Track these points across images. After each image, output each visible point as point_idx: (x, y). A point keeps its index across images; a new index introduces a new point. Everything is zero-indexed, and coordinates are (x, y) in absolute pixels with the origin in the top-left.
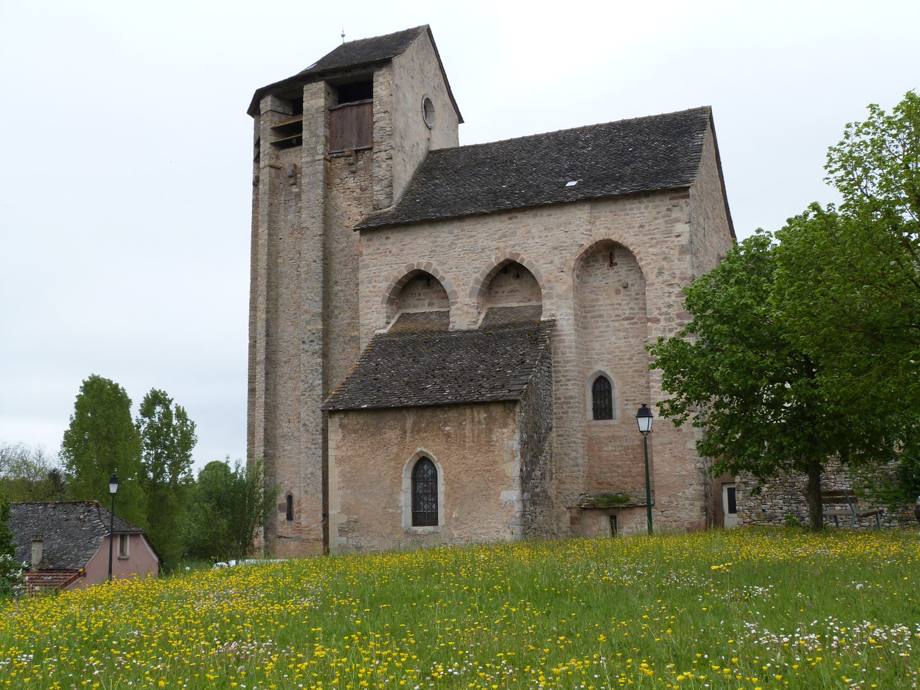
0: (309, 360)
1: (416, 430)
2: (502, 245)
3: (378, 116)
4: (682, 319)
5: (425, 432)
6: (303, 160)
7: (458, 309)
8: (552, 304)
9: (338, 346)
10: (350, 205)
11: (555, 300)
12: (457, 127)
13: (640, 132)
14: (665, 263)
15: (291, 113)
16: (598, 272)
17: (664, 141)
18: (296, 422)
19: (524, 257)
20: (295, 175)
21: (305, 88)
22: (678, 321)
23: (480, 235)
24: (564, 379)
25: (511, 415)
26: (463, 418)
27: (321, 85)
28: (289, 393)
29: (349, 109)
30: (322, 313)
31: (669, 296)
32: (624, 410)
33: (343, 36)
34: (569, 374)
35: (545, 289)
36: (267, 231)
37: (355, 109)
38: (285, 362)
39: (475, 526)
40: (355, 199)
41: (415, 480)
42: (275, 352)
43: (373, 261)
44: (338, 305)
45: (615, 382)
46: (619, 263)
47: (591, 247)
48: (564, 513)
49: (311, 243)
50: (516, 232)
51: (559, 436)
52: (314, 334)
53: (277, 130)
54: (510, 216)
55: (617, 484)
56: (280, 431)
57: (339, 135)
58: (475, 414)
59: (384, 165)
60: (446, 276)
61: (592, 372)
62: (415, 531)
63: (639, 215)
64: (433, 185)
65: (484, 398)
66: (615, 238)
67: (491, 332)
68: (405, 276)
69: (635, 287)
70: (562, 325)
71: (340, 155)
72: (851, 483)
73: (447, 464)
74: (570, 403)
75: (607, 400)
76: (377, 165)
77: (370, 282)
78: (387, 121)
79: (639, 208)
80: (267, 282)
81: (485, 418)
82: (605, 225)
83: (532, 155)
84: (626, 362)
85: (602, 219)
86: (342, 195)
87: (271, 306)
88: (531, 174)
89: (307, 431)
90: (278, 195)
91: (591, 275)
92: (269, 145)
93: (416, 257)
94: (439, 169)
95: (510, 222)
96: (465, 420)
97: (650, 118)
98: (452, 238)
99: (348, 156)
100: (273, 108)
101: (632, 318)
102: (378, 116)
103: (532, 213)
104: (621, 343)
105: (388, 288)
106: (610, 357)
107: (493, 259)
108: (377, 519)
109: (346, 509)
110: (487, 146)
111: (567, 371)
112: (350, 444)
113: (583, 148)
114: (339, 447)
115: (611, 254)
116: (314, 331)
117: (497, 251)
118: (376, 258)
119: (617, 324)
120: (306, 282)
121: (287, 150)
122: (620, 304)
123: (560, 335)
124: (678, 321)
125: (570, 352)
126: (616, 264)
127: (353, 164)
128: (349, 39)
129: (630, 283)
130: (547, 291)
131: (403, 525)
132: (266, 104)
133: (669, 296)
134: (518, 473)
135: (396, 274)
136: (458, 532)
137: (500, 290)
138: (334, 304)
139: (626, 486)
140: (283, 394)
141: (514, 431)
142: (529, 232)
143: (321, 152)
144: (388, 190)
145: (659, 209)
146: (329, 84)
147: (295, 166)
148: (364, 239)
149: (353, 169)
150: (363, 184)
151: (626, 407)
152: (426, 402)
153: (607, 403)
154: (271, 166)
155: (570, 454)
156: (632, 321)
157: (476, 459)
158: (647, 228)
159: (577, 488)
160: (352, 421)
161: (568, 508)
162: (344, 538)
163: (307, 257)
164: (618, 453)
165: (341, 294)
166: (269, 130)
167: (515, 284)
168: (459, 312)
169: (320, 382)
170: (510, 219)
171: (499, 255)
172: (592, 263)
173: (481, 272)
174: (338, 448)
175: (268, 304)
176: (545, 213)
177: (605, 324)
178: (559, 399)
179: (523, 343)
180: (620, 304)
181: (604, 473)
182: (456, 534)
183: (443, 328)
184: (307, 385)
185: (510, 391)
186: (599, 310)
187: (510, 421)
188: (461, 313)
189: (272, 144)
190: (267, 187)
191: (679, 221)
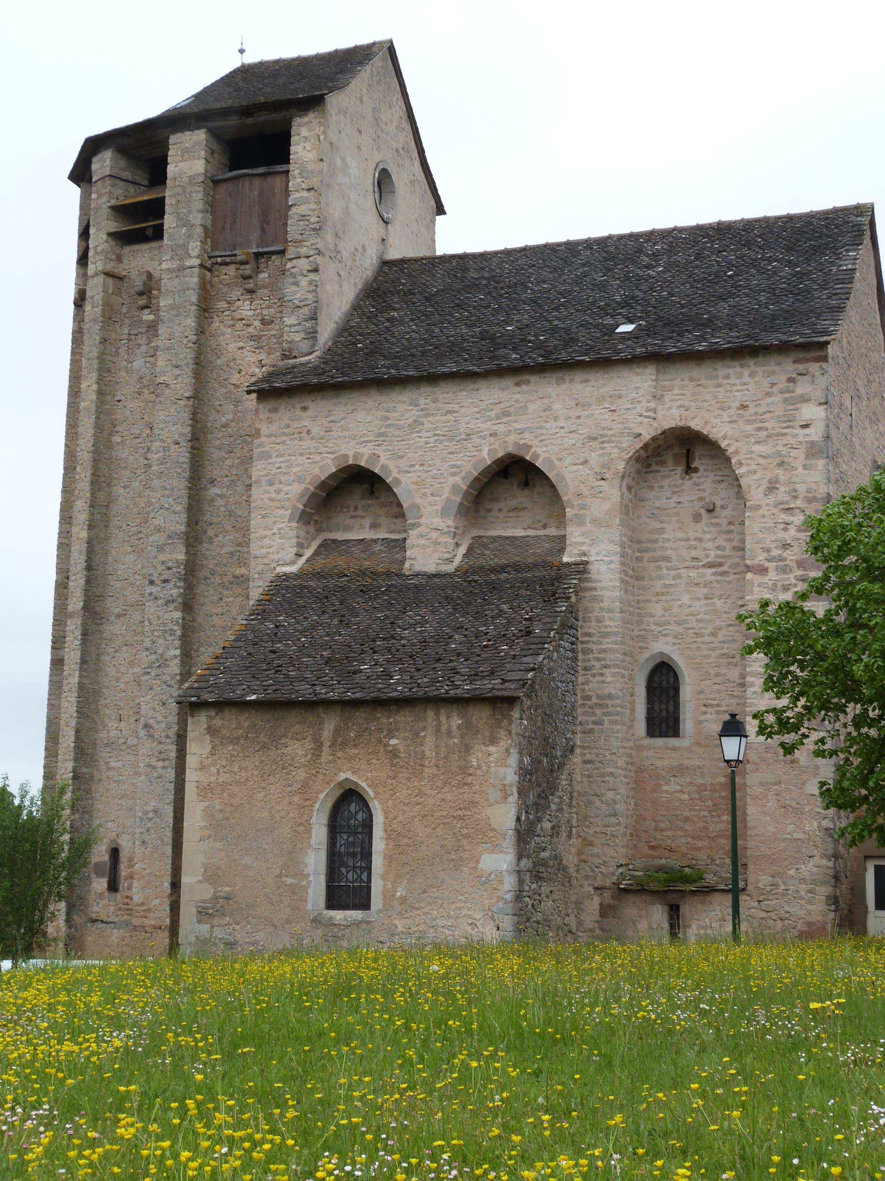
0: (160, 614)
1: (340, 742)
2: (501, 428)
3: (298, 195)
4: (805, 569)
5: (355, 746)
6: (164, 266)
7: (421, 536)
8: (583, 534)
10: (242, 348)
11: (589, 527)
12: (433, 222)
13: (748, 244)
14: (780, 472)
15: (146, 183)
16: (665, 483)
19: (539, 451)
21: (173, 139)
22: (799, 573)
23: (463, 410)
24: (597, 665)
25: (505, 723)
26: (421, 725)
27: (200, 136)
28: (123, 669)
29: (247, 180)
30: (186, 534)
31: (785, 529)
32: (700, 722)
33: (242, 51)
34: (608, 656)
35: (572, 507)
36: (95, 387)
37: (257, 181)
38: (118, 616)
39: (435, 912)
40: (252, 338)
42: (101, 597)
43: (277, 447)
44: (214, 520)
45: (686, 674)
46: (701, 468)
47: (654, 439)
48: (589, 897)
49: (172, 410)
50: (525, 408)
51: (585, 762)
52: (169, 568)
56: (103, 734)
57: (228, 226)
58: (443, 719)
59: (304, 282)
60: (402, 477)
61: (647, 655)
62: (331, 918)
64: (388, 320)
65: (459, 691)
66: (696, 425)
67: (476, 578)
71: (228, 259)
73: (390, 803)
74: (607, 706)
76: (291, 280)
78: (313, 206)
79: (740, 376)
80: (93, 474)
82: (679, 403)
83: (560, 276)
84: (707, 639)
85: (676, 391)
86: (229, 330)
87: (98, 517)
88: (556, 309)
89: (151, 736)
90: (117, 326)
91: (651, 488)
92: (105, 237)
93: (353, 443)
94: (398, 292)
95: (517, 389)
96: (424, 729)
97: (766, 219)
98: (414, 414)
99: (243, 263)
101: (721, 565)
102: (298, 195)
103: (555, 376)
104: (699, 606)
105: (302, 495)
106: (679, 629)
107: (485, 453)
109: (212, 876)
111: (604, 651)
112: (224, 763)
113: (649, 267)
115: (688, 451)
116: (170, 564)
117: (492, 440)
118: (283, 443)
120: (160, 478)
121: (136, 247)
122: (700, 540)
123: (595, 589)
124: (799, 573)
125: (611, 619)
126: (696, 470)
127: (250, 277)
128: (252, 58)
129: (719, 504)
131: (309, 907)
133: (785, 529)
134: (513, 825)
135: (317, 471)
136: (404, 921)
137: (495, 506)
138: (207, 517)
139: (698, 854)
140: (111, 671)
142: (548, 408)
143: (195, 253)
145: (774, 379)
146: (214, 133)
149: (251, 286)
150: (265, 312)
151: (702, 718)
153: (671, 709)
154: (107, 274)
155: (603, 795)
156: (720, 570)
157: (440, 796)
158: (752, 410)
160: (228, 721)
161: (597, 889)
163: (165, 434)
164: (686, 797)
165: (220, 502)
166: (105, 211)
167: (521, 498)
168: (422, 541)
169: (178, 652)
170: (517, 384)
171: (496, 446)
172: (655, 467)
173: (463, 474)
174: (202, 768)
176: (579, 376)
177: (672, 573)
178: (588, 698)
179: (531, 600)
180: (700, 540)
182: (400, 925)
183: (394, 568)
185: (504, 681)
186: (663, 548)
187: (502, 733)
188: (427, 543)
189: (110, 234)
190: (98, 310)
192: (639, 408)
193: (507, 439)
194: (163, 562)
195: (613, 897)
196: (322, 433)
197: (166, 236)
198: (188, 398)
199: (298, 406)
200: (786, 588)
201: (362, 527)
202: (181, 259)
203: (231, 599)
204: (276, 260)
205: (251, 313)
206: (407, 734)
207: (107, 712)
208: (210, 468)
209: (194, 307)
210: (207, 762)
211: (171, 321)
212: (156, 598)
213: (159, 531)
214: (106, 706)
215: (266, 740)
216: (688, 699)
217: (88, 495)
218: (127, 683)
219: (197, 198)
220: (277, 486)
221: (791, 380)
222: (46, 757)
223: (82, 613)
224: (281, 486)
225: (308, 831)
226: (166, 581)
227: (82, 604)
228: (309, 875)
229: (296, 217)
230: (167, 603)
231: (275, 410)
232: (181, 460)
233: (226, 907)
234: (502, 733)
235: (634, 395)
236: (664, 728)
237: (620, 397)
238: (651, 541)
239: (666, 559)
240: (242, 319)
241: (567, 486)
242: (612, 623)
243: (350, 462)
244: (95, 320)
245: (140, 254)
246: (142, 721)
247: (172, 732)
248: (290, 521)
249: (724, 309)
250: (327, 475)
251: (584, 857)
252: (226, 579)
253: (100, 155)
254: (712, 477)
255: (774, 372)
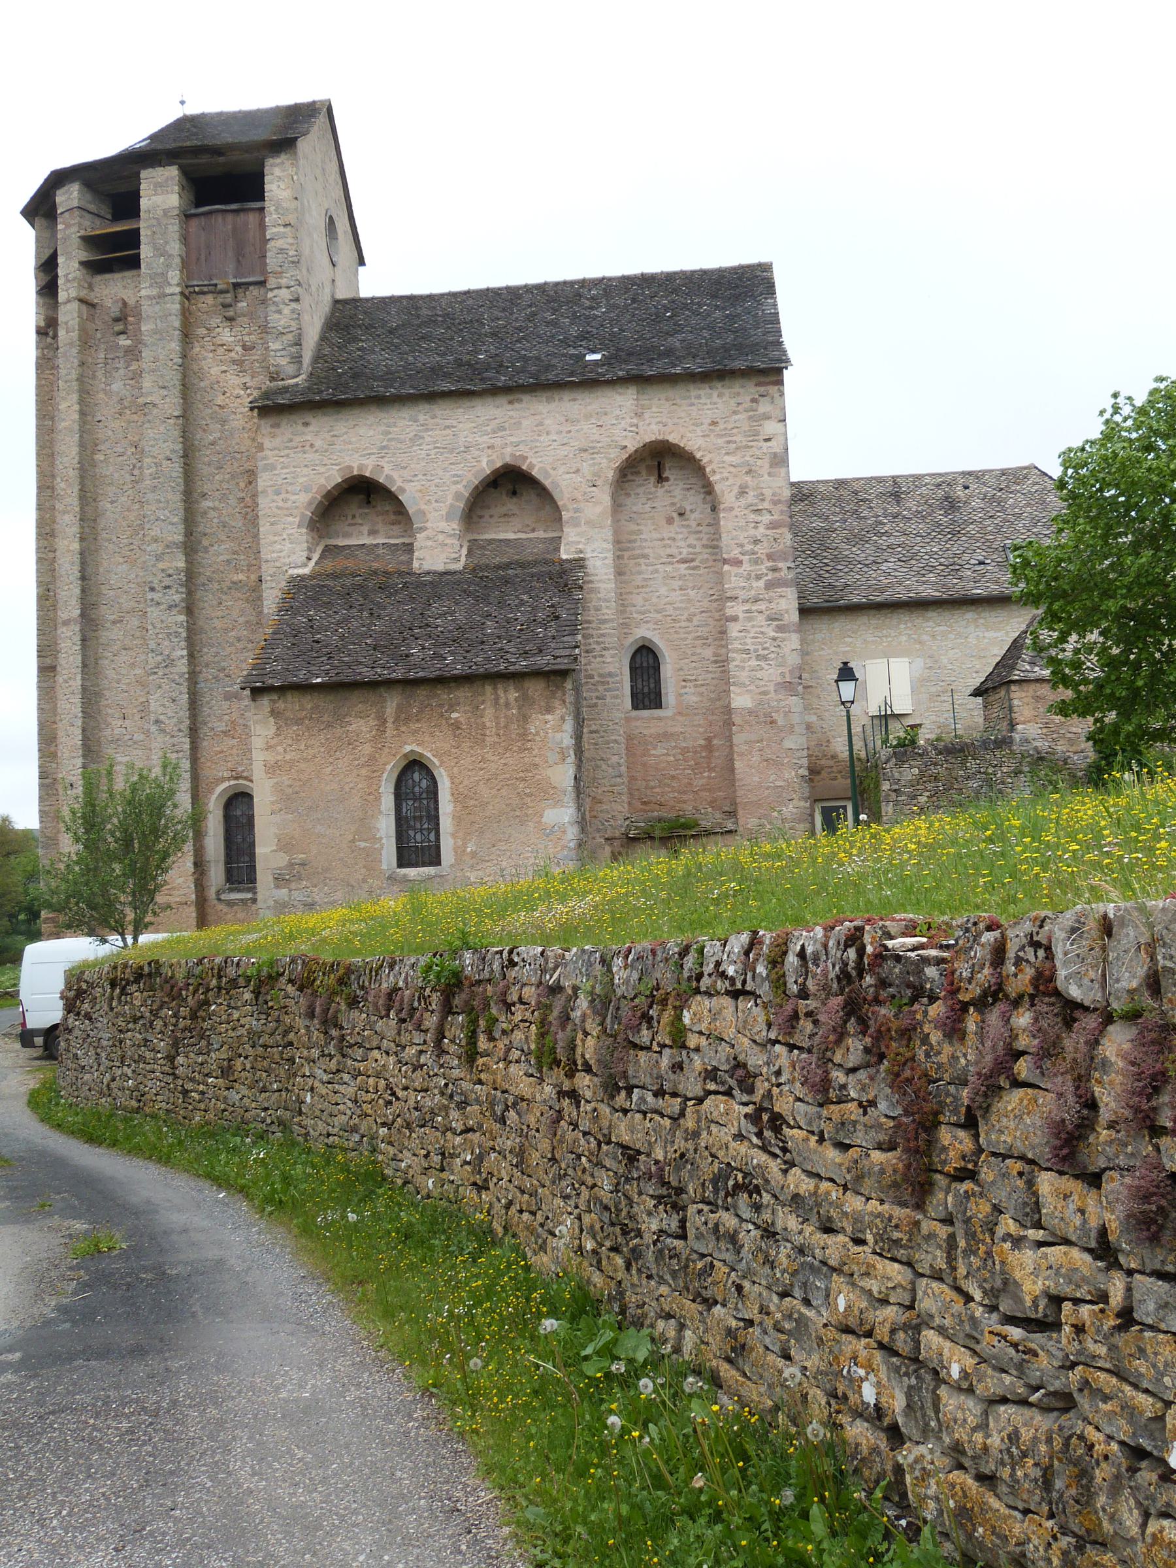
0: (163, 618)
1: (403, 718)
2: (498, 442)
3: (275, 230)
4: (774, 561)
5: (418, 721)
6: (143, 293)
8: (578, 534)
9: (211, 597)
10: (225, 372)
11: (584, 528)
13: (675, 291)
14: (748, 478)
15: (109, 217)
16: (641, 490)
17: (717, 306)
18: (137, 717)
19: (534, 461)
20: (124, 319)
21: (144, 174)
22: (769, 564)
24: (598, 648)
25: (559, 694)
26: (481, 699)
27: (173, 172)
28: (124, 672)
29: (220, 218)
30: (185, 543)
31: (756, 528)
32: (681, 695)
33: (182, 103)
34: (607, 640)
35: (568, 511)
36: (77, 407)
37: (230, 218)
38: (114, 622)
39: (504, 863)
40: (234, 362)
41: (399, 796)
42: (94, 605)
43: (282, 460)
44: (208, 531)
45: (666, 654)
46: (672, 478)
47: (636, 451)
48: (601, 847)
49: (162, 428)
50: (520, 423)
51: (591, 732)
52: (170, 576)
53: (90, 241)
54: (511, 397)
55: (672, 803)
56: (108, 732)
57: (203, 257)
58: (501, 692)
59: (286, 311)
60: (406, 486)
61: (631, 639)
62: (405, 875)
63: (709, 406)
64: (359, 349)
65: (517, 667)
66: (673, 438)
67: (486, 574)
68: (338, 485)
69: (696, 515)
70: (594, 566)
71: (205, 289)
72: (1032, 788)
73: (456, 770)
74: (608, 683)
75: (652, 681)
76: (273, 308)
77: (278, 493)
78: (290, 241)
79: (710, 396)
81: (516, 699)
82: (658, 419)
83: (511, 314)
84: (683, 624)
85: (654, 409)
86: (211, 355)
87: (87, 530)
88: (518, 341)
89: (163, 731)
90: (92, 350)
91: (628, 495)
92: (77, 265)
93: (356, 456)
94: (359, 326)
95: (510, 407)
96: (483, 702)
97: (683, 273)
98: (415, 428)
99: (222, 292)
100: (84, 204)
101: (692, 560)
102: (275, 230)
104: (676, 596)
105: (310, 503)
106: (659, 616)
107: (484, 464)
108: (341, 859)
109: (285, 845)
110: (430, 297)
111: (603, 635)
112: (290, 742)
113: (592, 308)
114: (271, 747)
115: (659, 463)
116: (171, 572)
117: (490, 451)
118: (288, 456)
119: (669, 568)
121: (108, 276)
122: (674, 539)
124: (769, 564)
125: (607, 607)
126: (667, 479)
127: (230, 306)
128: (192, 109)
129: (688, 508)
130: (571, 514)
131: (384, 867)
132: (69, 197)
133: (756, 528)
134: (572, 782)
135: (322, 481)
136: (476, 873)
137: (486, 513)
138: (201, 528)
139: (685, 806)
140: (111, 673)
141: (563, 719)
142: (541, 424)
143: (175, 281)
144: (293, 350)
145: (739, 400)
146: (185, 172)
147: (125, 304)
148: (265, 425)
149: (231, 314)
150: (246, 338)
151: (683, 691)
152: (421, 674)
153: (652, 686)
155: (609, 759)
156: (692, 564)
157: (503, 761)
158: (721, 426)
159: (620, 808)
160: (292, 704)
161: (607, 839)
162: (285, 891)
163: (155, 451)
164: (672, 759)
165: (212, 514)
166: (75, 241)
167: (511, 505)
168: (430, 543)
169: (185, 652)
170: (510, 402)
171: (494, 457)
172: (630, 477)
173: (464, 483)
174: (269, 747)
175: (82, 527)
176: (567, 395)
177: (650, 568)
178: (592, 677)
179: (546, 590)
180: (674, 539)
181: (653, 788)
182: (473, 876)
183: (403, 568)
184: (159, 658)
185: (555, 658)
187: (557, 703)
188: (434, 544)
189: (82, 263)
190: (75, 335)
191: (769, 418)
192: (623, 424)
193: (504, 451)
194: (163, 570)
195: (622, 846)
196: (326, 447)
197: (143, 266)
198: (177, 417)
199: (300, 422)
200: (758, 577)
201: (361, 533)
202: (160, 287)
203: (230, 603)
204: (254, 291)
205: (232, 339)
206: (467, 708)
207: (110, 711)
208: (200, 483)
209: (177, 332)
210: (273, 742)
211: (154, 344)
212: (158, 603)
213: (156, 541)
214: (107, 706)
215: (330, 719)
216: (669, 675)
217: (77, 509)
218: (129, 684)
219: (174, 228)
220: (283, 496)
221: (754, 400)
222: (40, 758)
223: (79, 619)
224: (288, 496)
225: (378, 799)
226: (166, 587)
227: (79, 612)
228: (381, 838)
229: (275, 250)
230: (170, 607)
231: (277, 426)
232: (174, 474)
233: (302, 872)
234: (557, 703)
235: (618, 412)
236: (647, 702)
237: (606, 414)
238: (630, 542)
239: (645, 556)
240: (222, 345)
241: (561, 491)
242: (609, 611)
243: (355, 473)
244: (71, 344)
245: (112, 283)
246: (153, 717)
247: (185, 726)
248: (299, 527)
249: (675, 342)
250: (333, 484)
251: (595, 813)
252: (224, 585)
253: (65, 188)
254: (681, 485)
255: (738, 394)
